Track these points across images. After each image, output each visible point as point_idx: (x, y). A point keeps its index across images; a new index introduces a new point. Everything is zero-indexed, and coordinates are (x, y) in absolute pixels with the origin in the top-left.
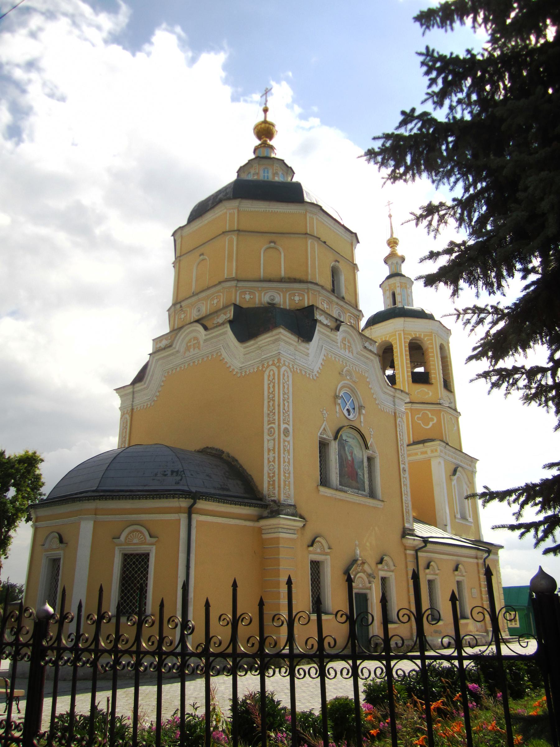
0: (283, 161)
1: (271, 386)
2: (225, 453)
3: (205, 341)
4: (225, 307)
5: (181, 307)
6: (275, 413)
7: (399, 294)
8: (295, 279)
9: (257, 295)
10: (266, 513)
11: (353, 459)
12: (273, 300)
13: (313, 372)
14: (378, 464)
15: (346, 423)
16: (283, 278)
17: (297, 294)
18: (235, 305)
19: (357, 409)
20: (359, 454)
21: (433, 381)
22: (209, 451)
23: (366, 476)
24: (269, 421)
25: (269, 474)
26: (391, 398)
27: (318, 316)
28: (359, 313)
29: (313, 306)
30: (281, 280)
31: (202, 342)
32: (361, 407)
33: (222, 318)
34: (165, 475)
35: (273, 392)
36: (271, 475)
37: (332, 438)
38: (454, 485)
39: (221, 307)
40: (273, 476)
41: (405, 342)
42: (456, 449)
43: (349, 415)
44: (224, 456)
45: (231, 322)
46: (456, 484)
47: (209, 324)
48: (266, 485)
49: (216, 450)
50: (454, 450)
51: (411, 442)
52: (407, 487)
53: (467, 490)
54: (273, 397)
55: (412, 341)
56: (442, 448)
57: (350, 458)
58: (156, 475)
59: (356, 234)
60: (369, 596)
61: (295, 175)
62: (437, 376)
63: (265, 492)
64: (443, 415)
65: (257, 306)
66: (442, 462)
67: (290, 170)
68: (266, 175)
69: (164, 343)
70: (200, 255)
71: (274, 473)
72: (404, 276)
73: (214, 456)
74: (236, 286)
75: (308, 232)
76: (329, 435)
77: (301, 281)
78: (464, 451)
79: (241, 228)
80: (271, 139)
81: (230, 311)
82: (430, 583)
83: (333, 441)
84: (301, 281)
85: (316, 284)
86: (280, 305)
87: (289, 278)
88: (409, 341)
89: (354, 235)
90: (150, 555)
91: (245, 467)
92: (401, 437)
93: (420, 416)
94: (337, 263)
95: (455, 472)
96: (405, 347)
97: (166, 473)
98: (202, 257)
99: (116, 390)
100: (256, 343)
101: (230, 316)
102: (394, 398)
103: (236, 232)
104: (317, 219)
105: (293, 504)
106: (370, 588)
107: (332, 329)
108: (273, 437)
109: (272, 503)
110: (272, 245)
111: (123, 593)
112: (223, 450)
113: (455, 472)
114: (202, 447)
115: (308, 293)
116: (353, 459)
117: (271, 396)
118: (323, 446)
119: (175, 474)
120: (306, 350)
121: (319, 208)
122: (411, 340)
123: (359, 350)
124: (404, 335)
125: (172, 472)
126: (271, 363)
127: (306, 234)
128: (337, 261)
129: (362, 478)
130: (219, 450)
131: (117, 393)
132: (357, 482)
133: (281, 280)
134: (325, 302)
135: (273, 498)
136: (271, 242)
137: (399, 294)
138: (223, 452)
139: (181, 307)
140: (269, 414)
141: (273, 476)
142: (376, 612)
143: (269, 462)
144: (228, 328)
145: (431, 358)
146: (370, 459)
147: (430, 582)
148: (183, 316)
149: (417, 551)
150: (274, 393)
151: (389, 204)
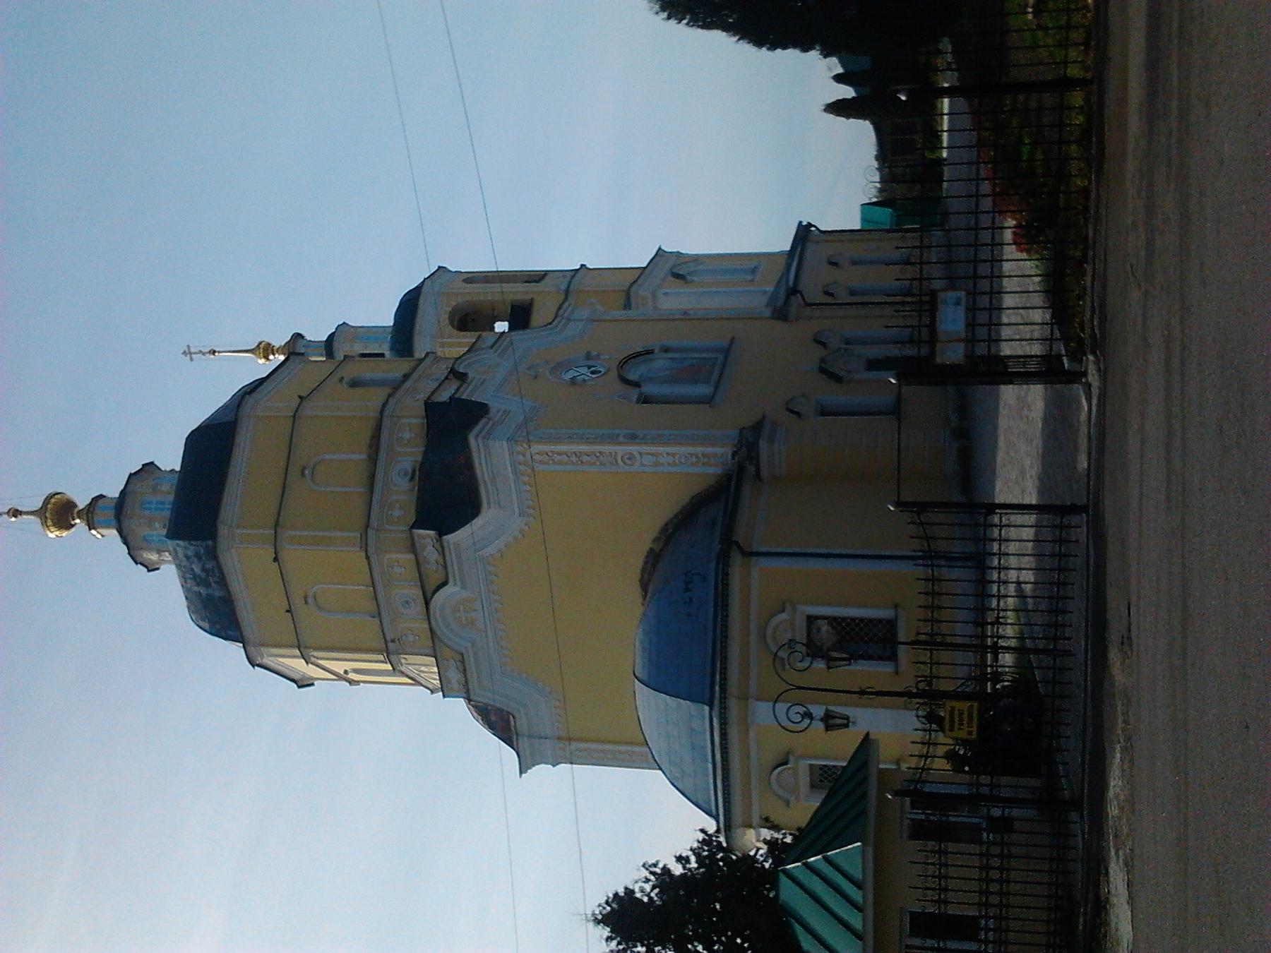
0: (131, 475)
1: (557, 458)
2: (652, 546)
3: (464, 587)
4: (413, 548)
5: (393, 641)
6: (600, 453)
8: (373, 438)
9: (394, 497)
10: (751, 469)
12: (406, 474)
14: (671, 343)
15: (614, 373)
16: (369, 457)
17: (400, 435)
18: (412, 527)
19: (590, 363)
20: (660, 363)
21: (528, 297)
22: (646, 577)
23: (695, 355)
24: (612, 463)
25: (692, 464)
26: (571, 323)
27: (444, 396)
29: (426, 403)
30: (373, 459)
31: (465, 594)
32: (588, 356)
33: (430, 553)
34: (691, 600)
35: (568, 456)
36: (694, 460)
37: (638, 390)
39: (412, 556)
40: (697, 457)
41: (457, 337)
43: (600, 372)
44: (657, 548)
45: (441, 534)
47: (434, 579)
48: (710, 470)
49: (646, 562)
54: (576, 455)
55: (455, 323)
58: (689, 615)
61: (156, 463)
62: (518, 292)
63: (719, 471)
65: (415, 499)
67: (147, 468)
68: (153, 506)
69: (454, 676)
70: (306, 603)
71: (691, 455)
72: (331, 336)
73: (654, 566)
74: (377, 530)
75: (292, 414)
76: (634, 394)
77: (378, 428)
78: (644, 265)
79: (272, 522)
80: (75, 506)
81: (421, 536)
82: (852, 293)
83: (641, 389)
84: (378, 428)
85: (384, 405)
86: (416, 461)
87: (370, 447)
88: (455, 331)
90: (810, 613)
91: (676, 510)
96: (464, 337)
97: (688, 601)
98: (310, 600)
99: (521, 772)
100: (485, 482)
101: (429, 536)
103: (279, 531)
105: (738, 431)
108: (638, 456)
109: (736, 459)
112: (648, 549)
114: (639, 588)
115: (399, 417)
117: (574, 459)
118: (645, 400)
119: (690, 586)
120: (500, 414)
121: (247, 396)
125: (687, 590)
126: (521, 457)
127: (294, 416)
128: (341, 379)
130: (646, 557)
131: (526, 772)
133: (373, 459)
134: (414, 396)
135: (730, 457)
136: (303, 474)
138: (651, 550)
139: (393, 641)
140: (601, 464)
141: (697, 457)
142: (866, 668)
143: (674, 464)
144: (450, 538)
145: (361, 490)
148: (411, 638)
150: (569, 455)
151: (188, 353)
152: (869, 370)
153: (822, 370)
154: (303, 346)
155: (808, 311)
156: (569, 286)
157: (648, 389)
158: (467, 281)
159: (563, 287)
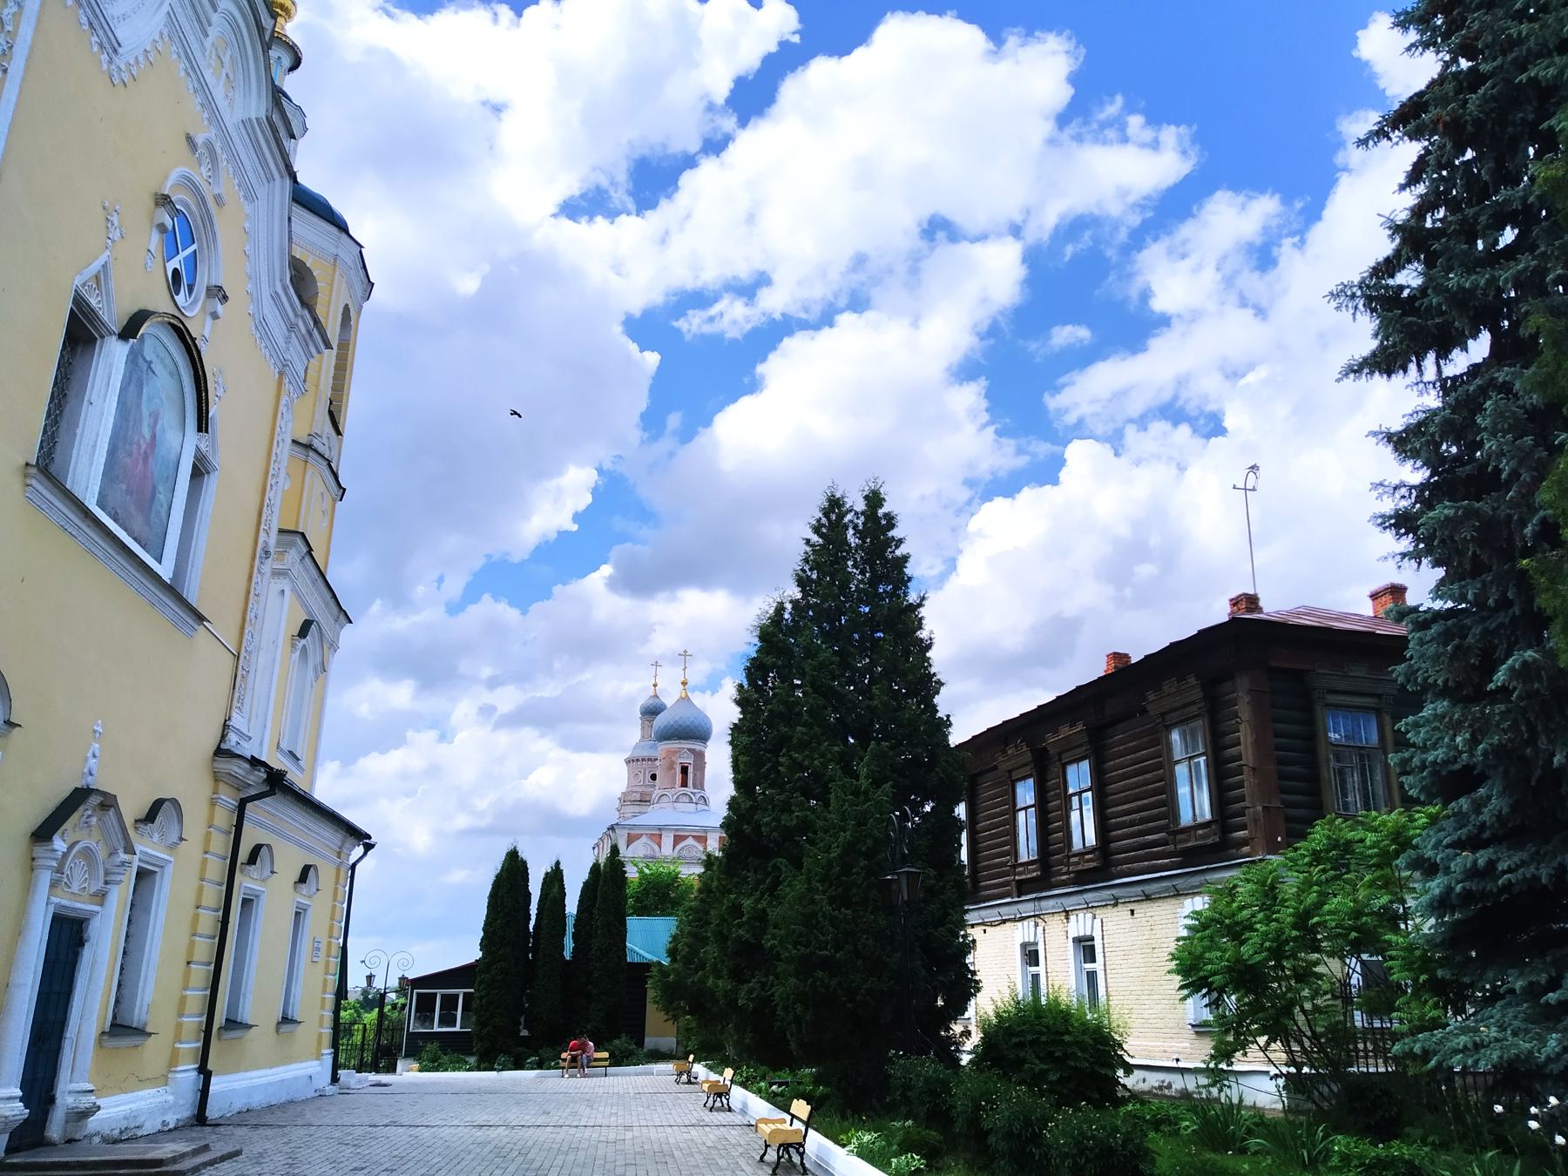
11: (154, 437)
13: (115, 51)
14: (212, 484)
66: (288, 592)
82: (247, 903)
116: (154, 437)
132: (148, 522)
146: (200, 471)
147: (247, 903)
153: (79, 796)
154: (279, 58)
155: (229, 798)
156: (316, 451)
157: (113, 357)
159: (316, 443)
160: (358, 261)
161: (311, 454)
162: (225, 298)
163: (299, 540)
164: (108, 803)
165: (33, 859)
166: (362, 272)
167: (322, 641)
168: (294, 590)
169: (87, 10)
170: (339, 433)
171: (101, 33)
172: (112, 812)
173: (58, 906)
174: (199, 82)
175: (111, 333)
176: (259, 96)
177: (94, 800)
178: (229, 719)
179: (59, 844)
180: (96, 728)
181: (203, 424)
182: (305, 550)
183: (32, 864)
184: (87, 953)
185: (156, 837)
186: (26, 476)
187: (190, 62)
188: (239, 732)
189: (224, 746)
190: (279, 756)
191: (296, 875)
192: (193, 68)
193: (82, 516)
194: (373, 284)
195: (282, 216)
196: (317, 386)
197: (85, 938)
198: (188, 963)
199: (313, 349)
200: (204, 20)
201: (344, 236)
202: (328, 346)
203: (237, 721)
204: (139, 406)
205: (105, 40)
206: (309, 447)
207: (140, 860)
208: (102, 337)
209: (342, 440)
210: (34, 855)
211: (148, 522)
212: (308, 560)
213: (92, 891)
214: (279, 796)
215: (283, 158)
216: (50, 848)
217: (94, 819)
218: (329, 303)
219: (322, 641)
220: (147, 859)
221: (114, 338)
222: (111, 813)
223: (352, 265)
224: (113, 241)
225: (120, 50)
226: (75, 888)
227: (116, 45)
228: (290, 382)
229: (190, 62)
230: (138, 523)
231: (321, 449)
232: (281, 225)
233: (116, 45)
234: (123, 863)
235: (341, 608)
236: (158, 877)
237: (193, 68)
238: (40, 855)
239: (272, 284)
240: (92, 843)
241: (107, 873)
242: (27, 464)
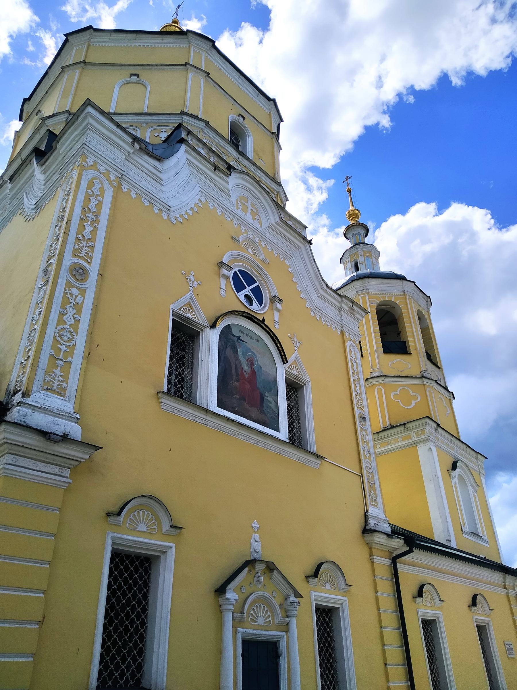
7: (362, 263)
28: (279, 187)
38: (455, 484)
42: (453, 436)
46: (457, 481)
50: (450, 437)
51: (388, 423)
52: (368, 445)
53: (474, 495)
55: (378, 309)
56: (433, 431)
57: (246, 368)
59: (274, 100)
60: (283, 646)
64: (429, 391)
66: (434, 449)
89: (272, 102)
92: (355, 368)
93: (398, 392)
94: (241, 119)
95: (454, 467)
102: (340, 311)
104: (206, 57)
106: (287, 628)
107: (388, 535)
110: (134, 78)
111: (141, 633)
113: (454, 467)
116: (253, 372)
122: (379, 305)
123: (273, 223)
124: (369, 299)
129: (275, 410)
137: (362, 263)
149: (394, 560)
152: (244, 642)
154: (359, 232)
156: (427, 378)
158: (421, 318)
159: (425, 374)
160: (416, 289)
161: (425, 380)
162: (280, 300)
163: (428, 421)
164: (271, 567)
165: (220, 606)
166: (421, 293)
167: (470, 471)
168: (437, 447)
169: (146, 197)
170: (439, 368)
171: (158, 204)
172: (275, 573)
173: (243, 634)
174: (232, 215)
175: (206, 327)
176: (273, 214)
177: (260, 567)
178: (367, 511)
179: (231, 595)
180: (253, 525)
181: (285, 361)
182: (435, 425)
183: (220, 610)
184: (283, 663)
185: (328, 586)
186: (159, 399)
187: (222, 207)
188: (375, 518)
189: (368, 528)
190: (464, 536)
191: (469, 601)
192: (225, 210)
193: (204, 413)
194: (429, 296)
195: (310, 261)
196: (416, 349)
197: (280, 653)
198: (386, 664)
199: (358, 316)
200: (225, 190)
201: (404, 282)
202: (367, 312)
203: (372, 511)
204: (237, 358)
205: (161, 207)
206: (423, 377)
207: (315, 600)
208: (202, 330)
209: (442, 371)
210: (220, 603)
211: (263, 412)
212: (440, 430)
213: (276, 622)
214: (416, 551)
215: (300, 236)
216: (225, 598)
217: (262, 579)
218: (408, 311)
219: (470, 471)
220: (423, 615)
221: (208, 329)
222: (275, 573)
223: (413, 292)
224: (193, 287)
225: (171, 209)
226: (261, 621)
227: (168, 208)
228: (349, 334)
229: (222, 207)
230: (254, 413)
231: (429, 376)
232: (311, 264)
233: (168, 208)
234: (292, 603)
235: (476, 452)
236: (167, 552)
237: (225, 210)
238: (222, 603)
239: (317, 292)
240: (266, 594)
241: (286, 611)
242: (448, 470)
